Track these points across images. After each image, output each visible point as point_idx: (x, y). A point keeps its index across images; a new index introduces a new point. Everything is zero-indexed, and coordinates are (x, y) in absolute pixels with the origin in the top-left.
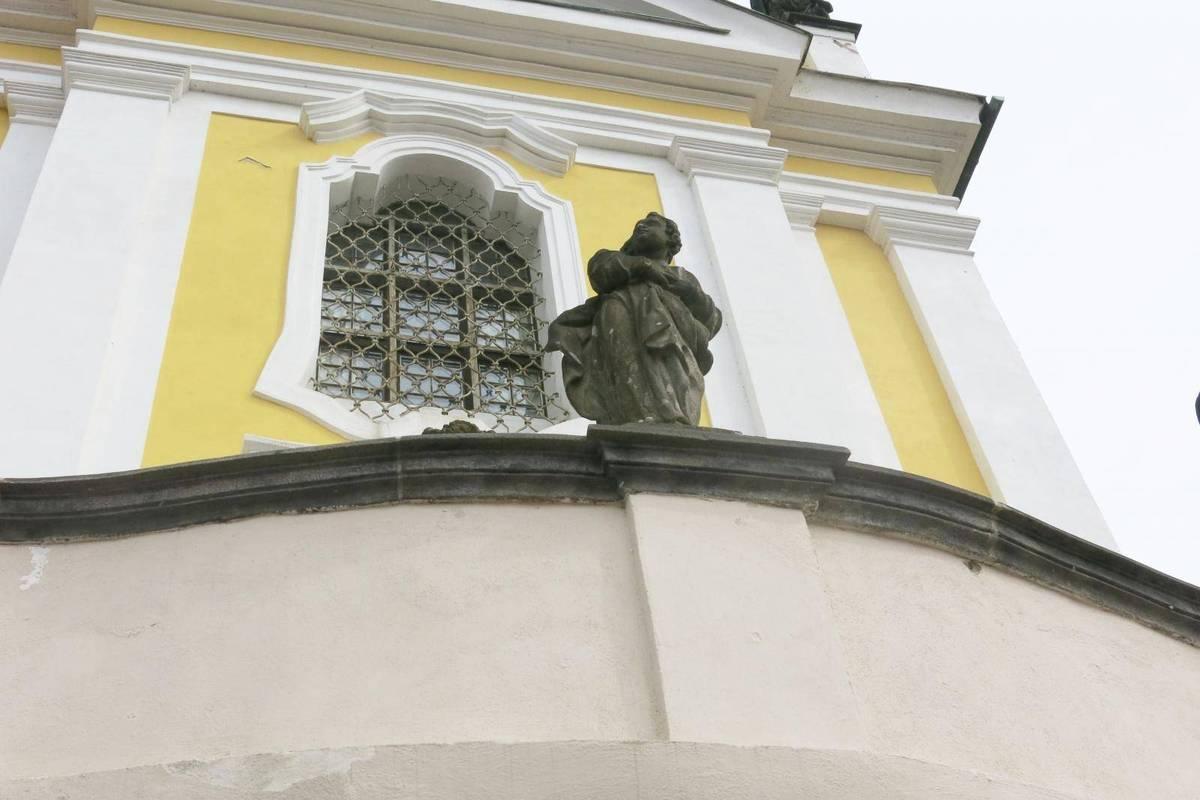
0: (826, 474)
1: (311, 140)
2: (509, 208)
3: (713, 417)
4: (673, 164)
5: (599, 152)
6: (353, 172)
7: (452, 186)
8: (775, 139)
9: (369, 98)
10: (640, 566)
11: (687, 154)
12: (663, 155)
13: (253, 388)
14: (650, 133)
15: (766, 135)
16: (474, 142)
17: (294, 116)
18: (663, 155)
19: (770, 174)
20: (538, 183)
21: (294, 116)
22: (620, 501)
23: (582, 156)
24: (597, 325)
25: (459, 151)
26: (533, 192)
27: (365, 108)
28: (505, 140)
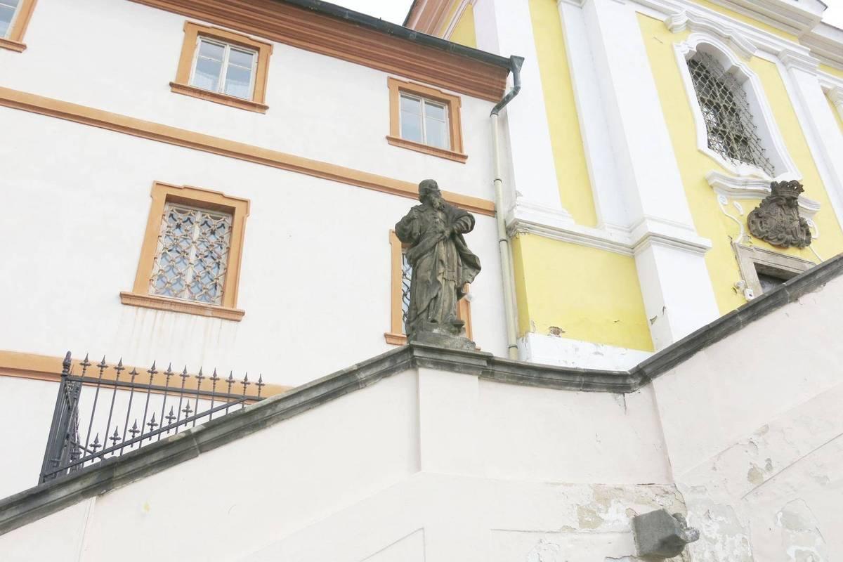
0: (484, 363)
1: (670, 30)
2: (733, 74)
3: (465, 144)
4: (780, 59)
5: (766, 54)
6: (689, 49)
7: (710, 57)
8: (813, 53)
9: (688, 14)
10: (181, 14)
11: (789, 57)
12: (776, 54)
13: (745, 298)
14: (760, 39)
15: (808, 50)
16: (719, 39)
17: (663, 18)
18: (776, 54)
19: (813, 70)
20: (745, 64)
21: (663, 18)
22: (417, 370)
23: (758, 53)
24: (513, 71)
25: (716, 43)
26: (745, 68)
27: (686, 19)
28: (730, 41)
